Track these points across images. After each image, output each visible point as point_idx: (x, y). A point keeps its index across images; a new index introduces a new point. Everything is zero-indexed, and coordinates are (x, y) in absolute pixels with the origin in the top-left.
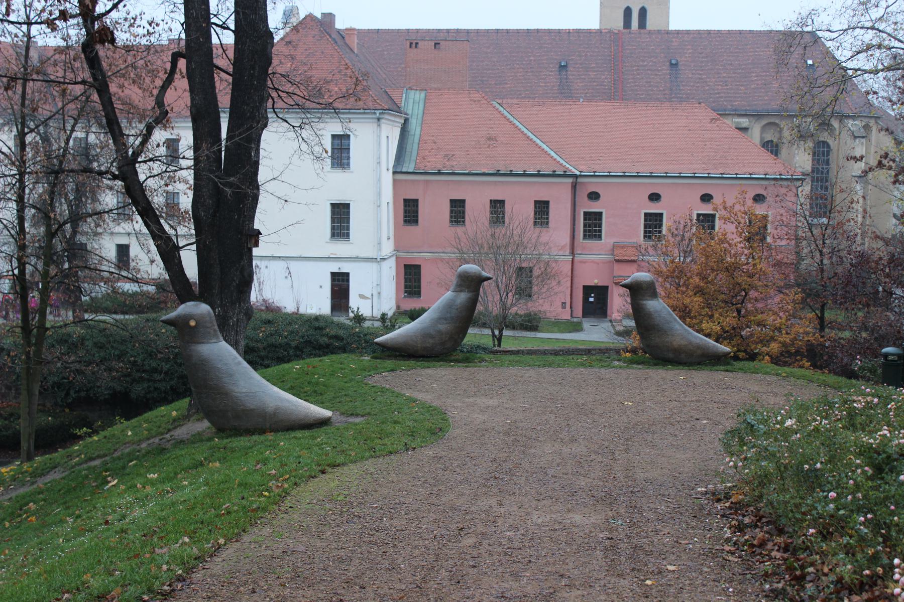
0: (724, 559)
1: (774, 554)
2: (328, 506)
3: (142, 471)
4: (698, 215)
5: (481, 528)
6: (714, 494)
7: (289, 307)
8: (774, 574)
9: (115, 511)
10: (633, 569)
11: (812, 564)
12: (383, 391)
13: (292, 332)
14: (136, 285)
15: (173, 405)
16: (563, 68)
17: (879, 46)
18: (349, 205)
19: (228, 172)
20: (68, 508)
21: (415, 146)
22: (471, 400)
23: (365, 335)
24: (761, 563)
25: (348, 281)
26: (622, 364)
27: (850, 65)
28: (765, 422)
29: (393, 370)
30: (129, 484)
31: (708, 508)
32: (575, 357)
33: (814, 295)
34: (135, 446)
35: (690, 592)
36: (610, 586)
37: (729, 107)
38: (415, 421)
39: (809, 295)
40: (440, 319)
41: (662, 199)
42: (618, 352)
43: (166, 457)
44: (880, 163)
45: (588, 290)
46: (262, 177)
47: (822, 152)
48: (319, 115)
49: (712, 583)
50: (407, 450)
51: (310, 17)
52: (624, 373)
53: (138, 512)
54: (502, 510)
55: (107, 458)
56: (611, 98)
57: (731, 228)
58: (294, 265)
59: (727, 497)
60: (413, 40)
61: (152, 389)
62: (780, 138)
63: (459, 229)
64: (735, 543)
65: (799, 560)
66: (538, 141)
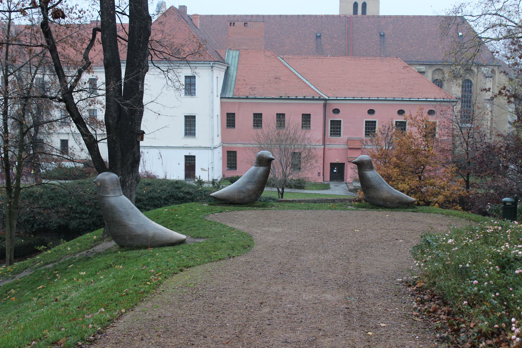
0: (413, 319)
1: (442, 316)
2: (184, 290)
3: (77, 270)
4: (396, 122)
5: (273, 302)
6: (407, 282)
7: (161, 176)
8: (442, 328)
9: (61, 294)
10: (361, 326)
11: (464, 322)
12: (216, 224)
13: (162, 190)
14: (73, 163)
15: (94, 232)
16: (318, 37)
17: (500, 25)
18: (195, 116)
19: (126, 97)
20: (34, 292)
21: (233, 83)
22: (266, 229)
23: (205, 192)
24: (434, 322)
25: (195, 160)
26: (353, 208)
27: (483, 35)
28: (437, 241)
29: (221, 212)
30: (69, 278)
31: (403, 290)
32: (326, 204)
33: (464, 168)
34: (72, 256)
35: (394, 339)
36: (348, 335)
37: (414, 60)
38: (234, 241)
39: (460, 168)
40: (248, 182)
41: (376, 113)
42: (350, 201)
43: (90, 262)
44: (500, 92)
45: (333, 165)
46: (145, 101)
47: (467, 86)
48: (178, 65)
49: (406, 334)
50: (230, 258)
51: (172, 8)
52: (354, 213)
53: (74, 294)
54: (285, 292)
55: (56, 263)
56: (346, 55)
57: (415, 129)
58: (163, 152)
59: (415, 284)
60: (232, 21)
61: (82, 223)
62: (443, 78)
63: (259, 131)
64: (419, 311)
65: (456, 320)
66: (304, 80)
